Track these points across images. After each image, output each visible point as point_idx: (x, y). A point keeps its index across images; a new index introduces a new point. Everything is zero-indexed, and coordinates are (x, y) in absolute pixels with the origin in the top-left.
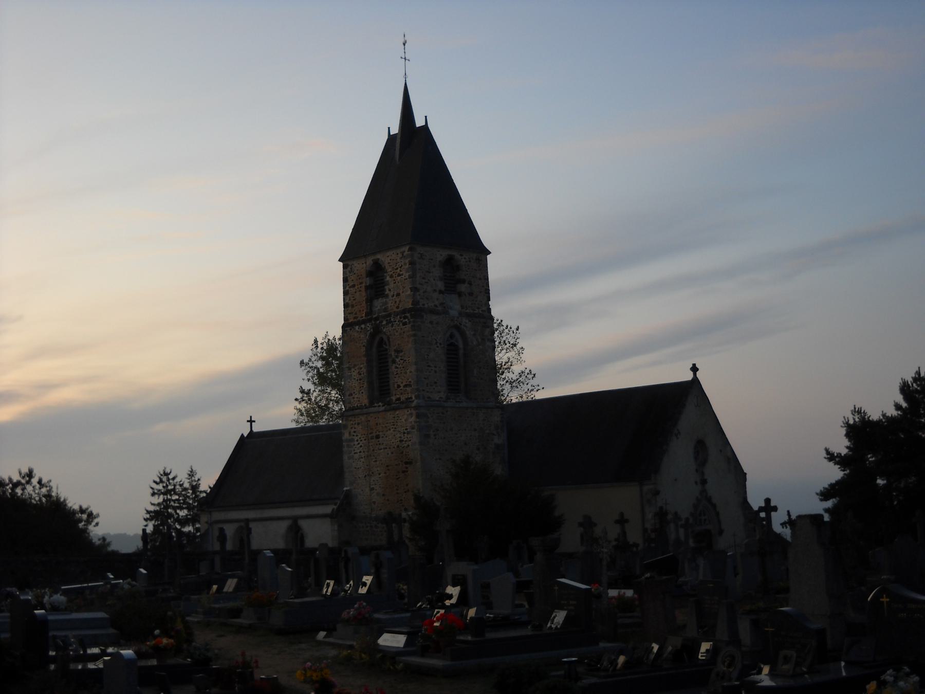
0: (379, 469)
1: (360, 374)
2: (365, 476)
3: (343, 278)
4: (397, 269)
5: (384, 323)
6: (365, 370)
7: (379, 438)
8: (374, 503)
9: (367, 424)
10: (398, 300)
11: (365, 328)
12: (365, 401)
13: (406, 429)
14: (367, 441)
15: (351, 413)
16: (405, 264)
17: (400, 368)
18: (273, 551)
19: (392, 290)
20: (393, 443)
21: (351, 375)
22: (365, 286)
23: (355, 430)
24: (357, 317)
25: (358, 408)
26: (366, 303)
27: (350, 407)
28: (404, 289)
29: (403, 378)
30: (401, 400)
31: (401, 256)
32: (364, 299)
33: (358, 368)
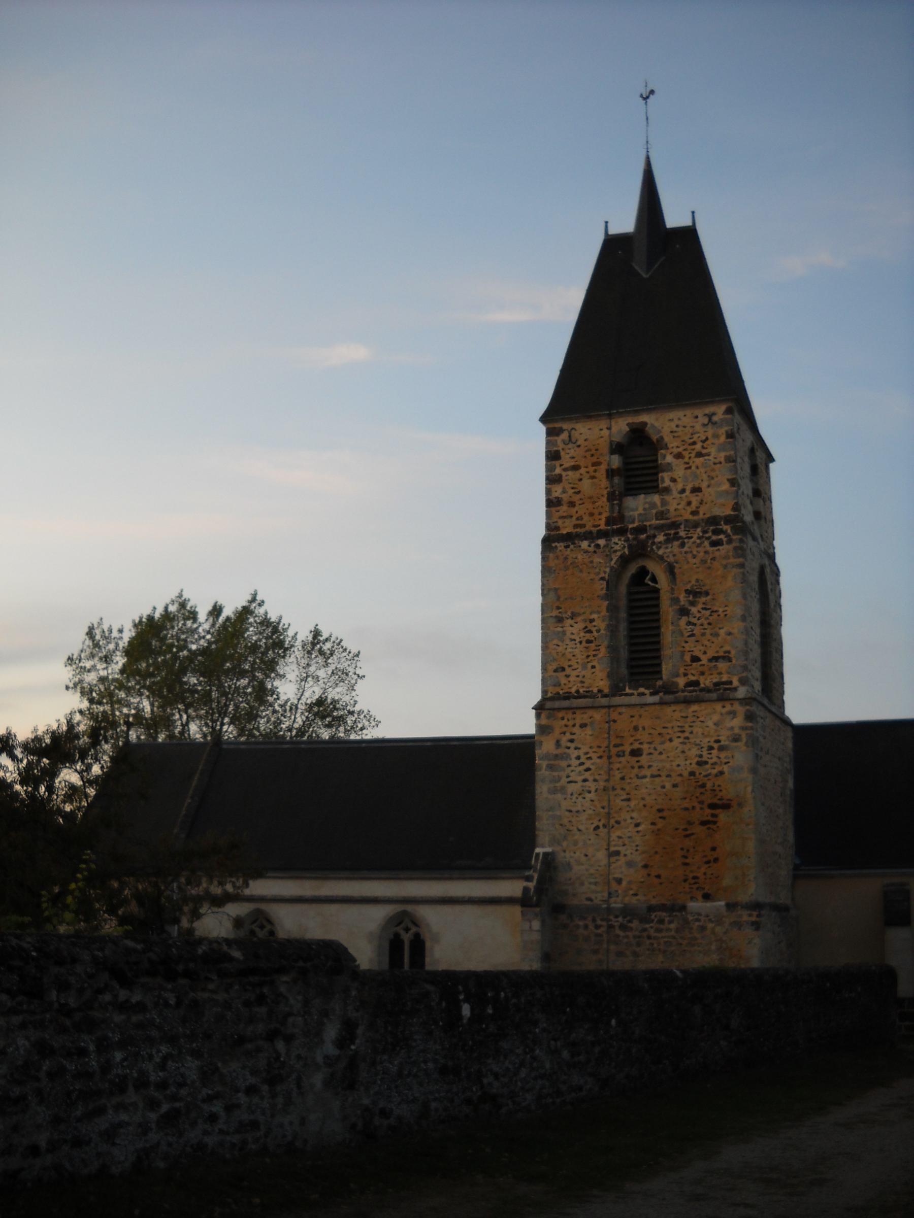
0: (634, 815)
1: (590, 632)
2: (597, 828)
3: (546, 452)
4: (694, 443)
5: (660, 538)
6: (603, 626)
7: (641, 755)
8: (619, 881)
9: (609, 727)
10: (695, 500)
11: (606, 546)
12: (599, 680)
13: (718, 741)
14: (605, 759)
15: (557, 704)
16: (716, 436)
17: (702, 625)
18: (682, 972)
19: (679, 480)
20: (678, 765)
21: (564, 633)
22: (607, 471)
23: (573, 737)
24: (584, 526)
25: (579, 696)
26: (608, 500)
27: (558, 693)
28: (713, 482)
29: (706, 643)
30: (702, 685)
31: (706, 421)
32: (605, 492)
33: (585, 621)
